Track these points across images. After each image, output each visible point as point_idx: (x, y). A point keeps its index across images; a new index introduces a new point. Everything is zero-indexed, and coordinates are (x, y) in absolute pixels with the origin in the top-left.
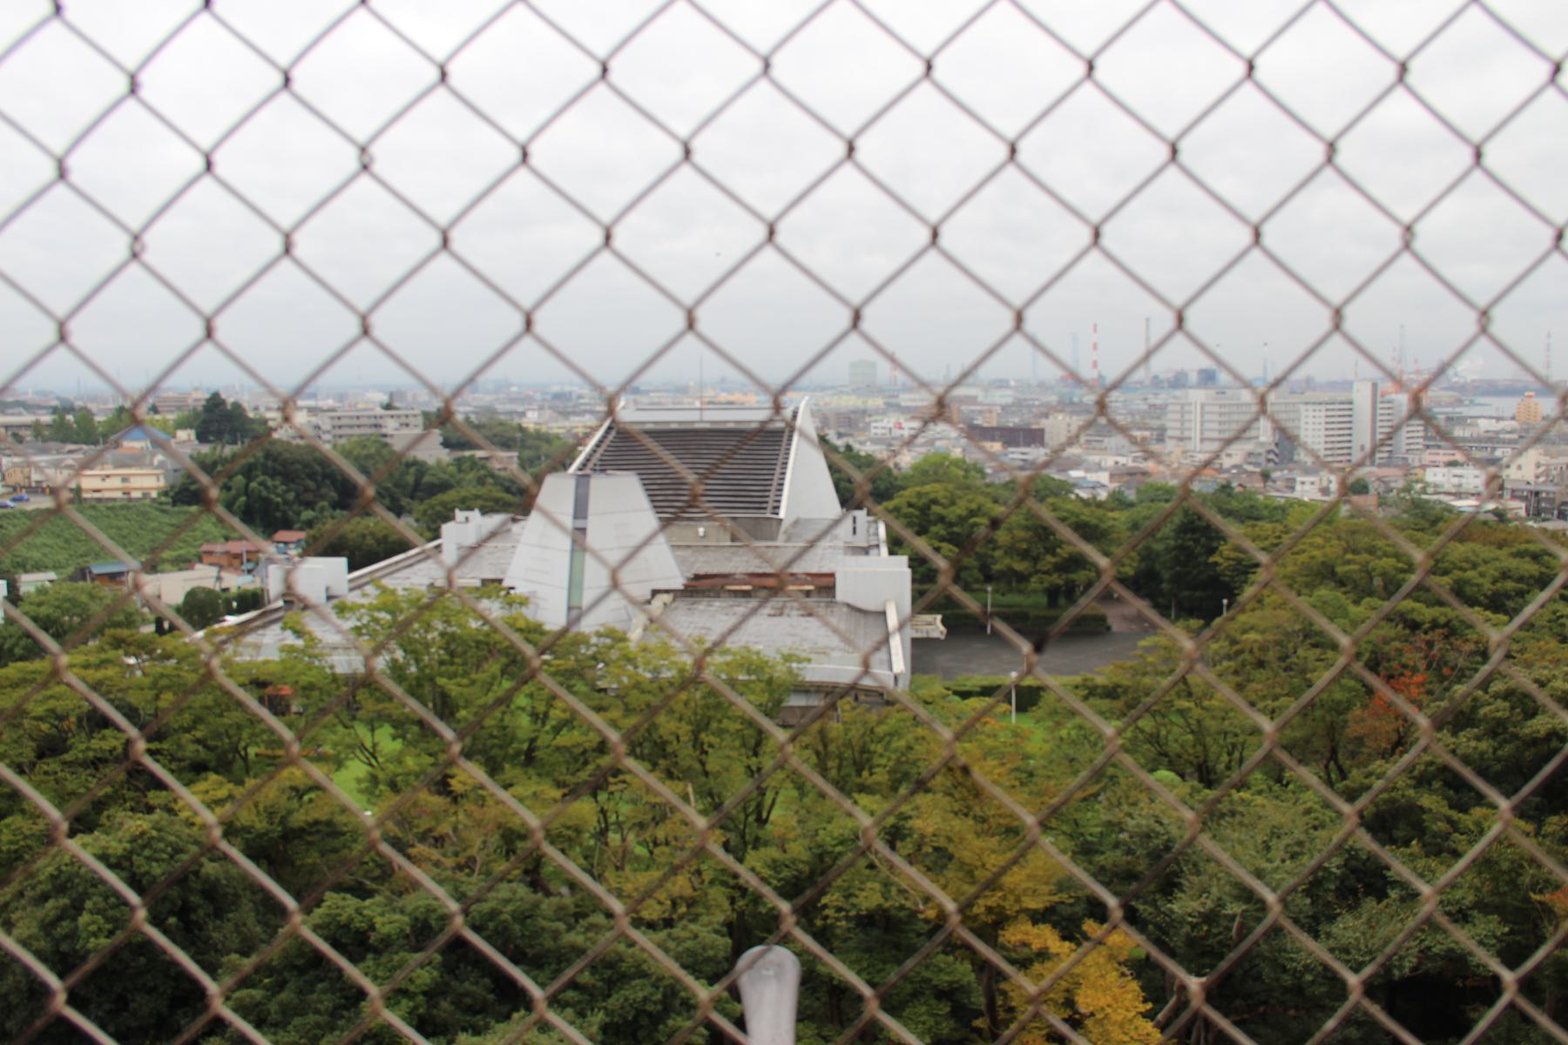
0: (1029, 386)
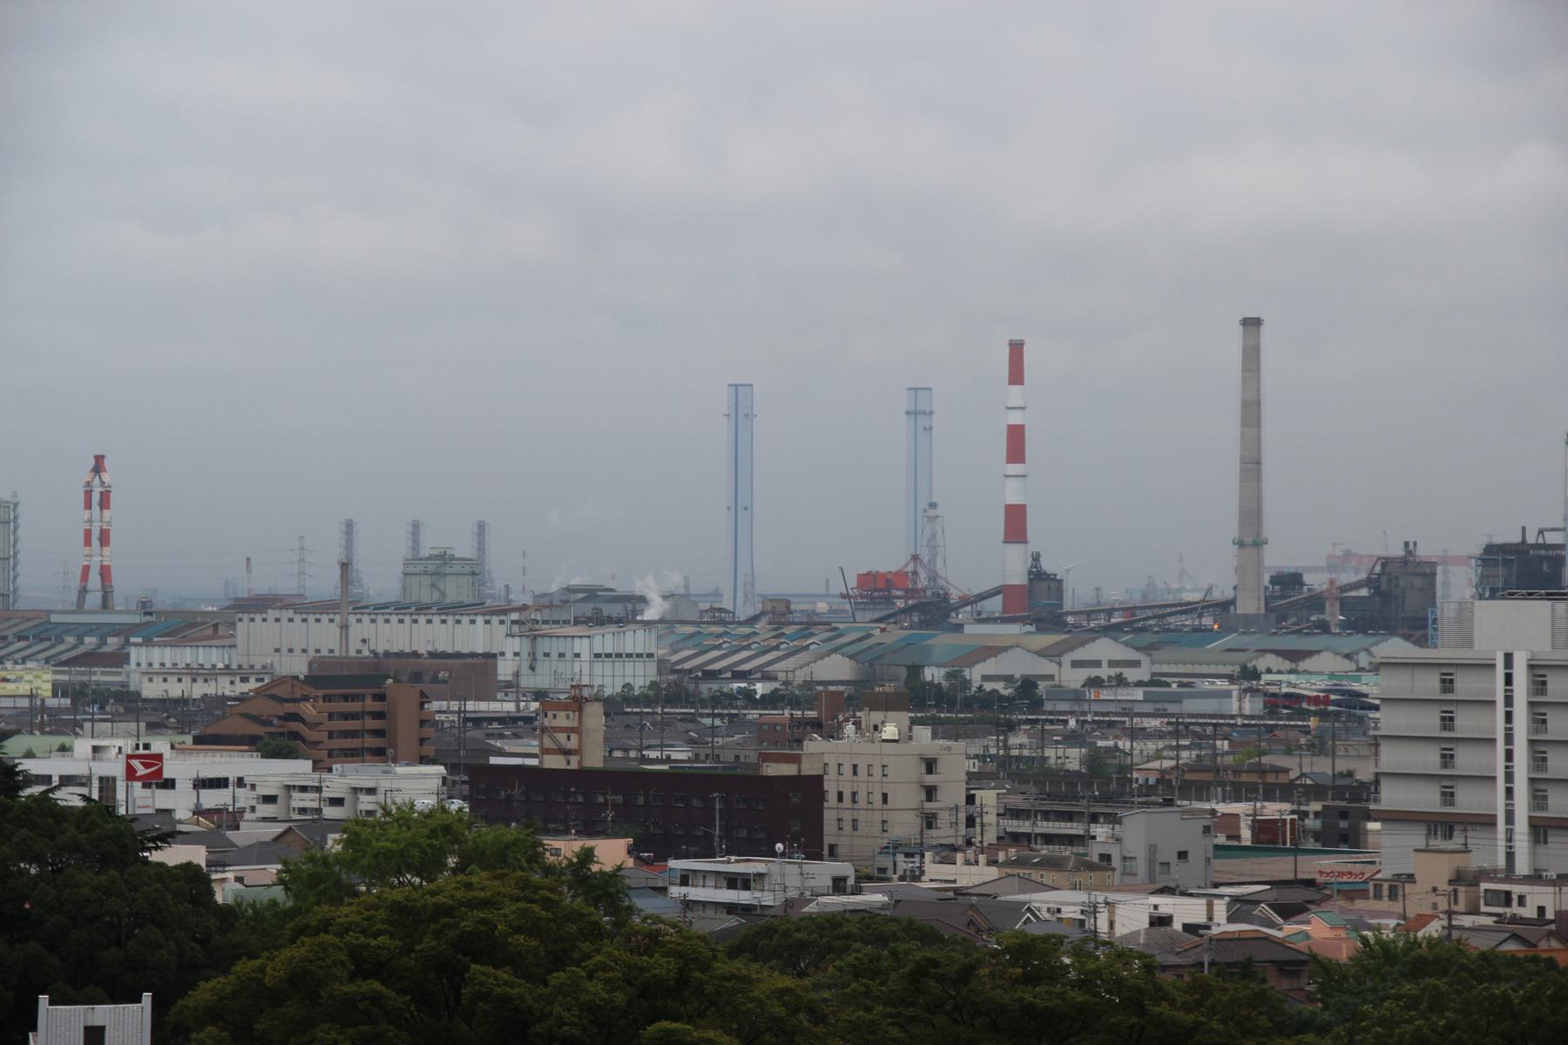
0: (719, 616)
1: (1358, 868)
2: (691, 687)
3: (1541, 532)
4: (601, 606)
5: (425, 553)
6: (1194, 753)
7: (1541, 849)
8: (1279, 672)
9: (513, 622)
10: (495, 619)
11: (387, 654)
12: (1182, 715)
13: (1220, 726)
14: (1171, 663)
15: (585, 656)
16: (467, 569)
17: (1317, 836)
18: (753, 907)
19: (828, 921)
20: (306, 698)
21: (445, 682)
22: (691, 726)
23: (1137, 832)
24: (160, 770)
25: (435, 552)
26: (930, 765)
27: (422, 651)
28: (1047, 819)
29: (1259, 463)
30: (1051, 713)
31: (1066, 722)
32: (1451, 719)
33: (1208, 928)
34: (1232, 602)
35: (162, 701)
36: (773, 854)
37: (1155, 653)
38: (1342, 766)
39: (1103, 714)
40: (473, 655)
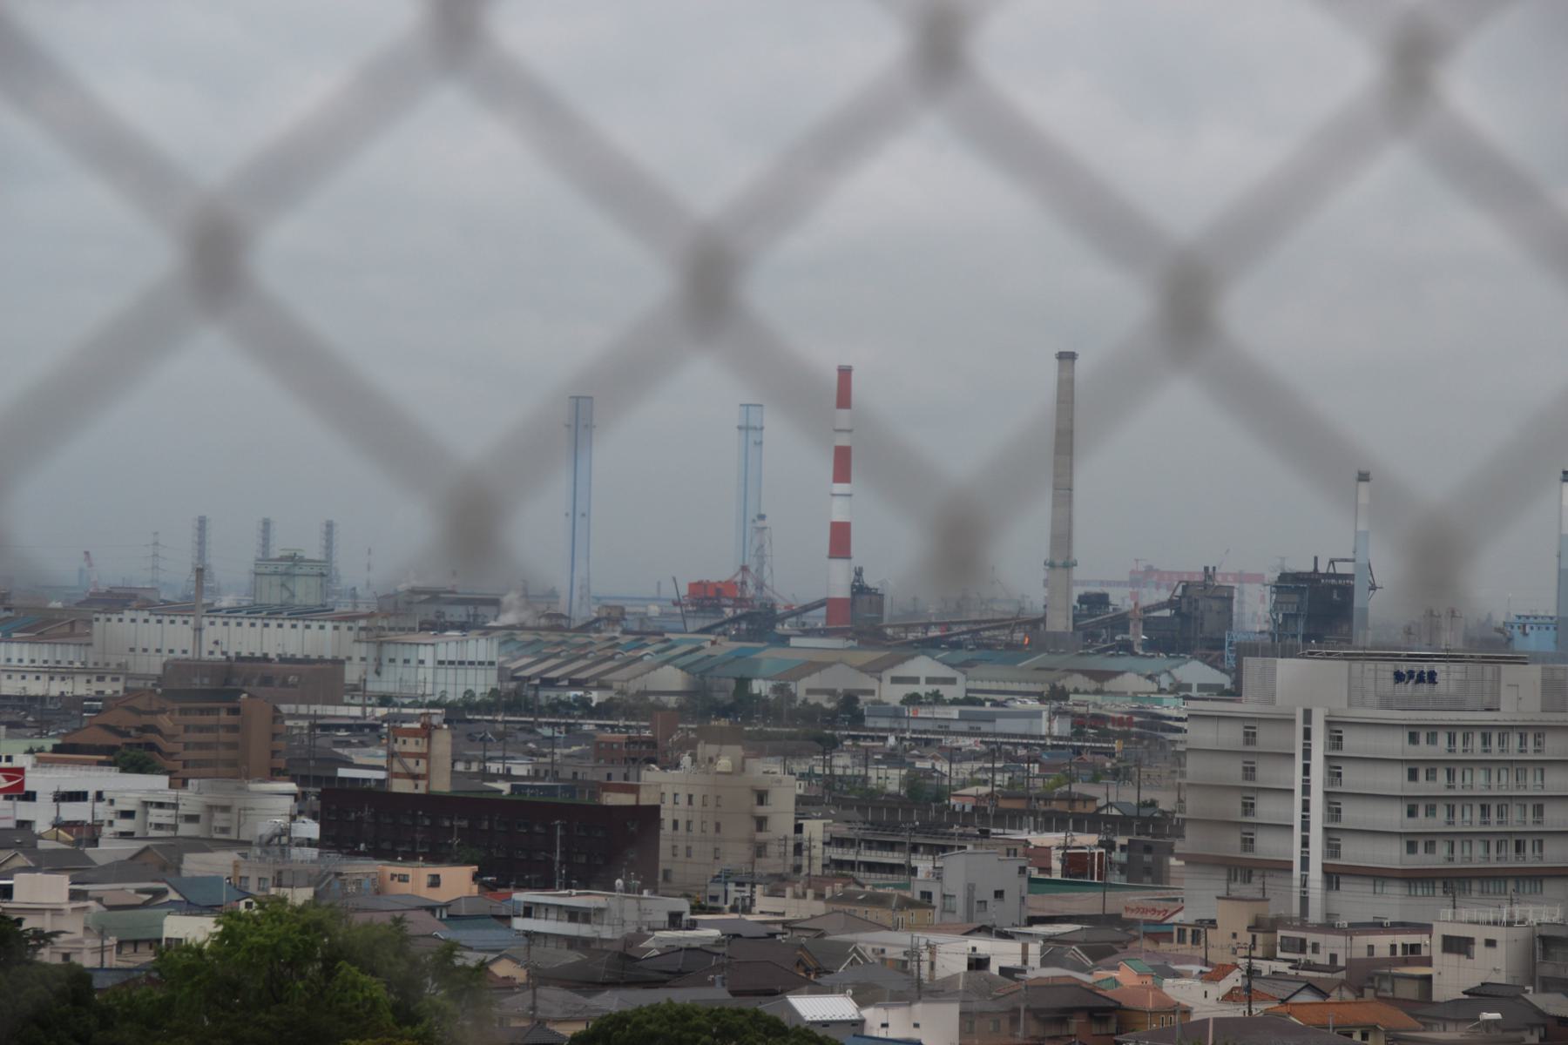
1: (1162, 906)
2: (531, 693)
3: (1332, 562)
4: (444, 608)
5: (276, 553)
6: (1007, 776)
7: (1334, 895)
8: (1086, 692)
9: (362, 629)
10: (344, 626)
11: (239, 658)
12: (995, 735)
13: (1032, 743)
14: (987, 679)
15: (429, 663)
16: (316, 571)
17: (1123, 869)
18: (593, 940)
19: (678, 1013)
20: (162, 711)
21: (294, 686)
22: (531, 736)
23: (958, 871)
24: (22, 783)
25: (286, 553)
26: (762, 797)
27: (272, 655)
28: (870, 848)
29: (1070, 490)
30: (872, 729)
31: (885, 739)
32: (1253, 769)
33: (1024, 972)
34: (1043, 620)
35: (21, 698)
36: (612, 889)
37: (969, 670)
38: (1146, 796)
39: (921, 732)
40: (321, 660)
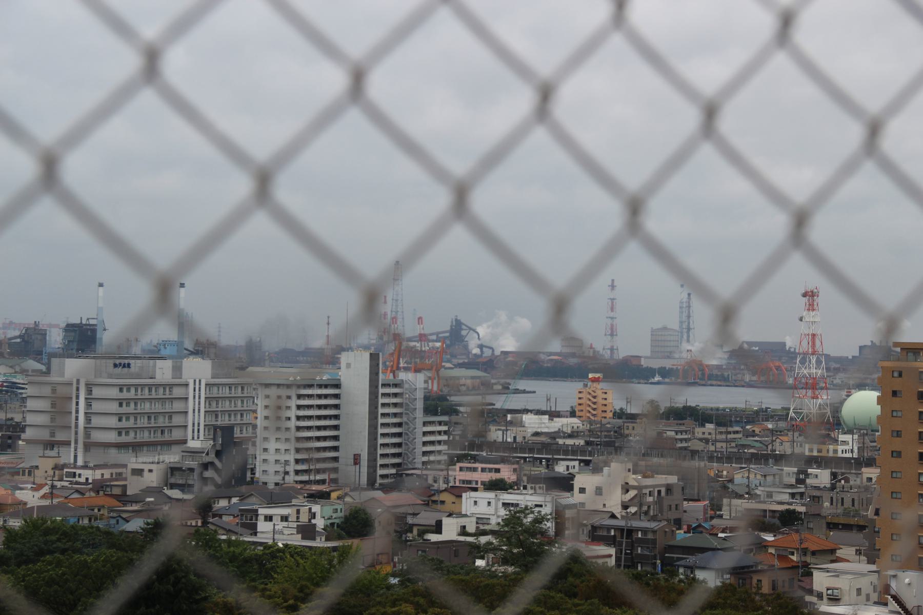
38: (9, 416)
